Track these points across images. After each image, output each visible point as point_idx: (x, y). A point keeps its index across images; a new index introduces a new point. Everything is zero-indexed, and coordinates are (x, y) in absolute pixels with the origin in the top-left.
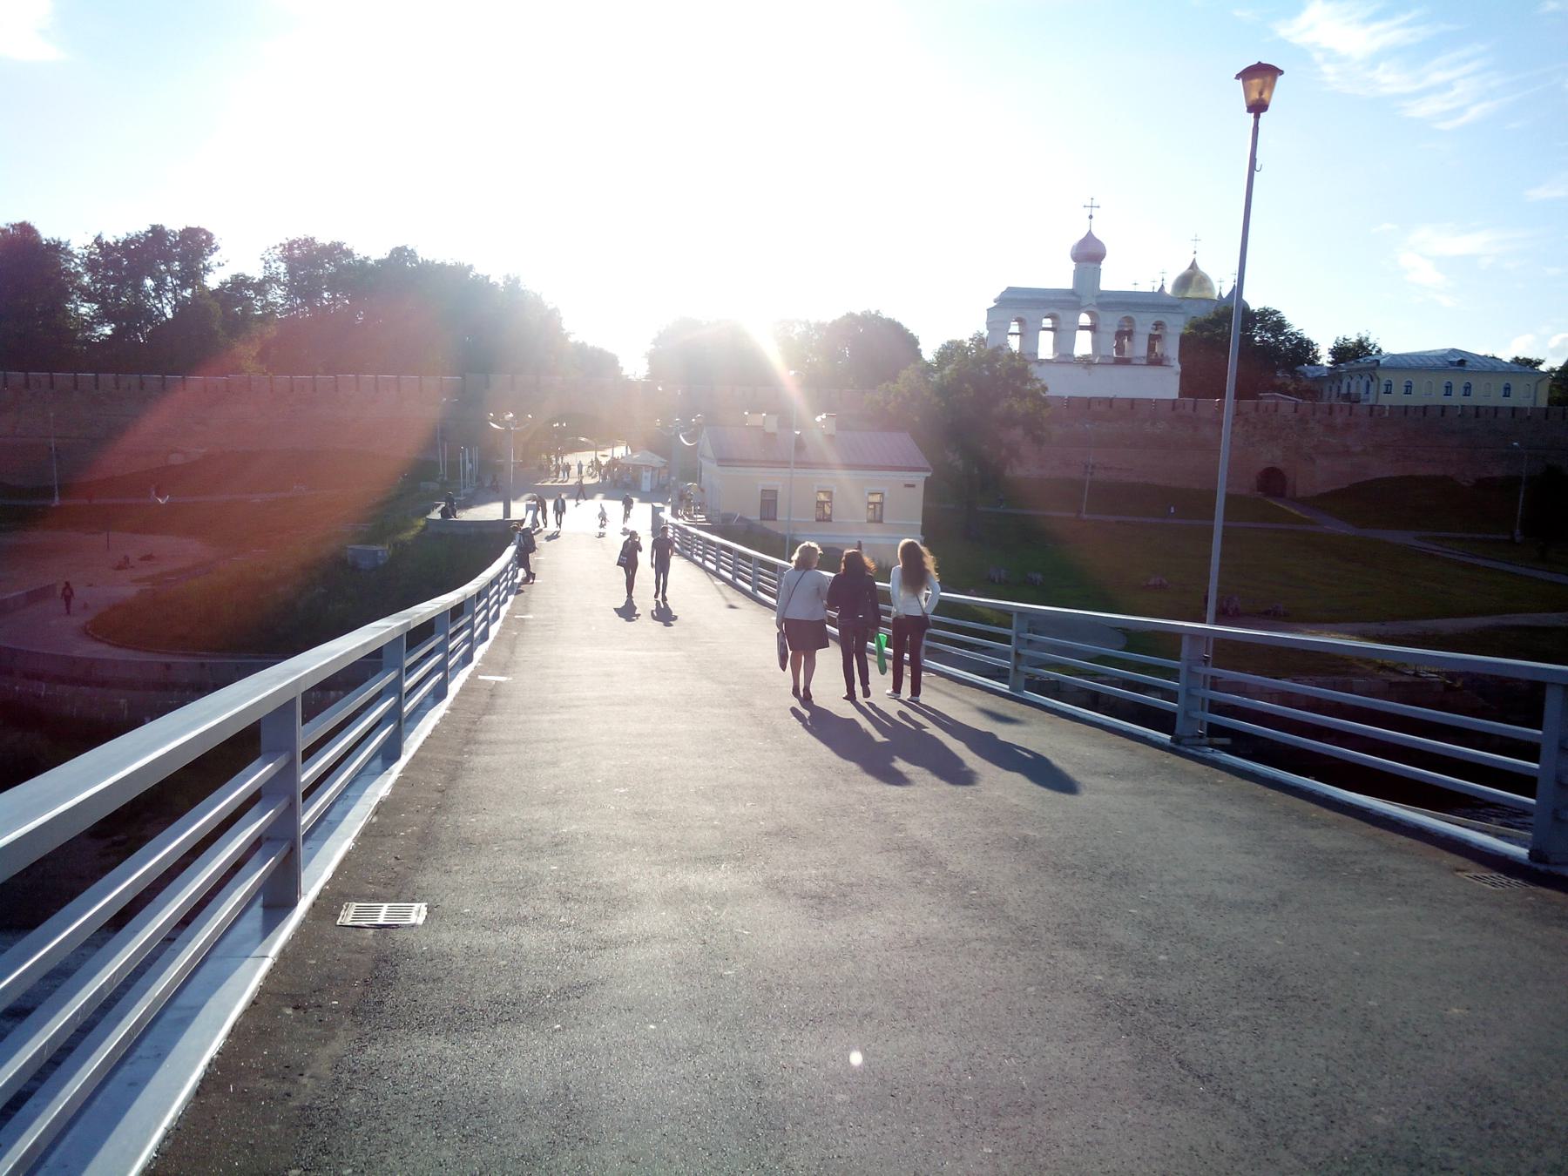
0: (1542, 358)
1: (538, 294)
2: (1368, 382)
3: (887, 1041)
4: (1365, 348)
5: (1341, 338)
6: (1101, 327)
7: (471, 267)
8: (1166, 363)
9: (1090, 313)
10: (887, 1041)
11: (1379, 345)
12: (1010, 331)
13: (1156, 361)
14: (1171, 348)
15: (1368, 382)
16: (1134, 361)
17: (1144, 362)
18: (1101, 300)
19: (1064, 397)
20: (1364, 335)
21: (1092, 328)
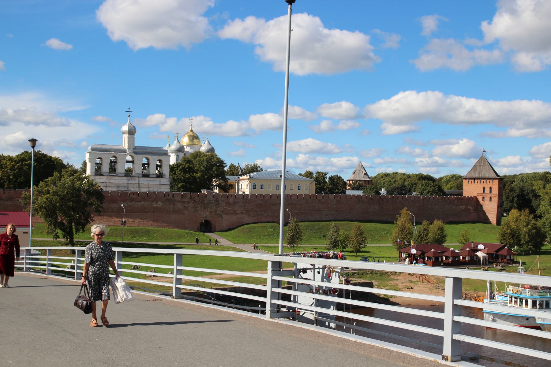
6: (135, 162)
15: (247, 184)
16: (151, 176)
18: (136, 150)
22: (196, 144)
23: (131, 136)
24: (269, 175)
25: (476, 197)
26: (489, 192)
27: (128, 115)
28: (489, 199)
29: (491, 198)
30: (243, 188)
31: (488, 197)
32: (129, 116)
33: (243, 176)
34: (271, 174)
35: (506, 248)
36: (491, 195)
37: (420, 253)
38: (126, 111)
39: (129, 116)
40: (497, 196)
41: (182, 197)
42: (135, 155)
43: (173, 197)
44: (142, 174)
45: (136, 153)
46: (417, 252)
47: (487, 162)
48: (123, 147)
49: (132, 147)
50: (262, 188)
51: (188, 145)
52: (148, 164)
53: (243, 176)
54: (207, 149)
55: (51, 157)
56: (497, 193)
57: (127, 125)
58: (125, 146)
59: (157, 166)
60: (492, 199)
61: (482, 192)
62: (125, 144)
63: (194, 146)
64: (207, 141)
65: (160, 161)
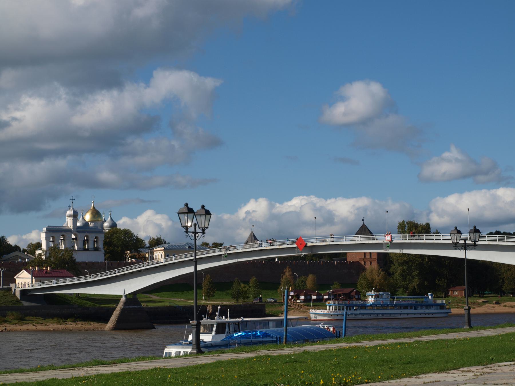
0: (222, 243)
1: (414, 222)
2: (162, 254)
3: (412, 371)
4: (160, 242)
5: (152, 238)
6: (78, 239)
7: (403, 221)
8: (99, 250)
9: (75, 235)
10: (412, 371)
11: (165, 240)
12: (50, 240)
13: (96, 249)
14: (101, 245)
15: (162, 254)
16: (89, 250)
17: (93, 250)
19: (99, 262)
20: (159, 236)
21: (53, 241)
22: (99, 220)
23: (74, 218)
24: (179, 247)
25: (359, 262)
26: (369, 256)
27: (72, 202)
28: (370, 263)
29: (371, 262)
30: (157, 257)
31: (369, 261)
32: (72, 203)
33: (157, 248)
34: (174, 245)
35: (355, 290)
36: (371, 260)
37: (296, 294)
38: (70, 199)
39: (72, 203)
40: (376, 260)
41: (118, 265)
42: (79, 234)
43: (112, 265)
44: (84, 249)
45: (79, 232)
46: (294, 294)
47: (367, 230)
48: (69, 227)
49: (76, 228)
50: (253, 226)
51: (91, 221)
52: (87, 240)
53: (157, 248)
54: (110, 224)
55: (417, 224)
56: (376, 258)
57: (72, 210)
58: (70, 227)
59: (94, 242)
60: (372, 263)
61: (363, 257)
62: (69, 223)
63: (98, 222)
64: (82, 216)
65: (96, 238)
